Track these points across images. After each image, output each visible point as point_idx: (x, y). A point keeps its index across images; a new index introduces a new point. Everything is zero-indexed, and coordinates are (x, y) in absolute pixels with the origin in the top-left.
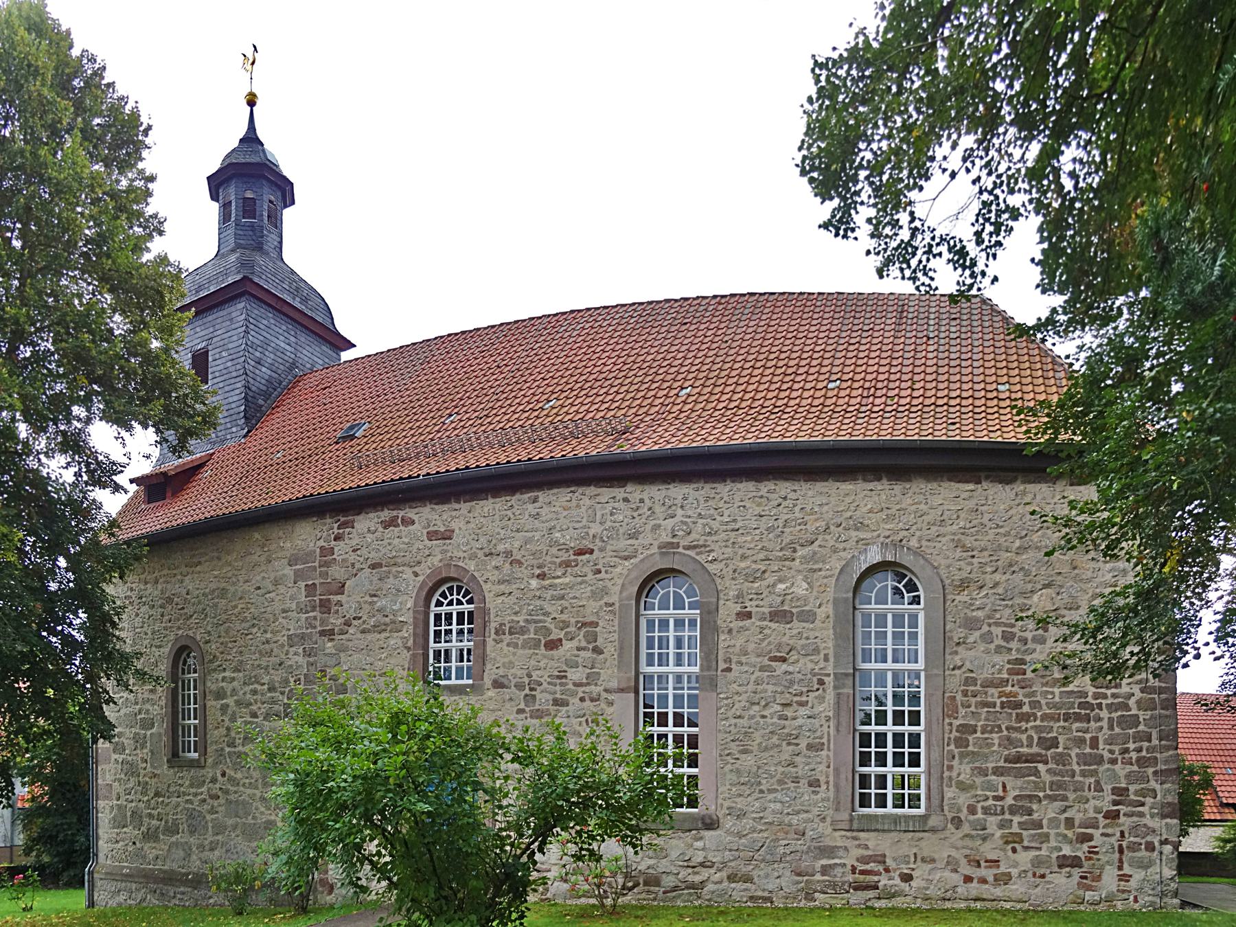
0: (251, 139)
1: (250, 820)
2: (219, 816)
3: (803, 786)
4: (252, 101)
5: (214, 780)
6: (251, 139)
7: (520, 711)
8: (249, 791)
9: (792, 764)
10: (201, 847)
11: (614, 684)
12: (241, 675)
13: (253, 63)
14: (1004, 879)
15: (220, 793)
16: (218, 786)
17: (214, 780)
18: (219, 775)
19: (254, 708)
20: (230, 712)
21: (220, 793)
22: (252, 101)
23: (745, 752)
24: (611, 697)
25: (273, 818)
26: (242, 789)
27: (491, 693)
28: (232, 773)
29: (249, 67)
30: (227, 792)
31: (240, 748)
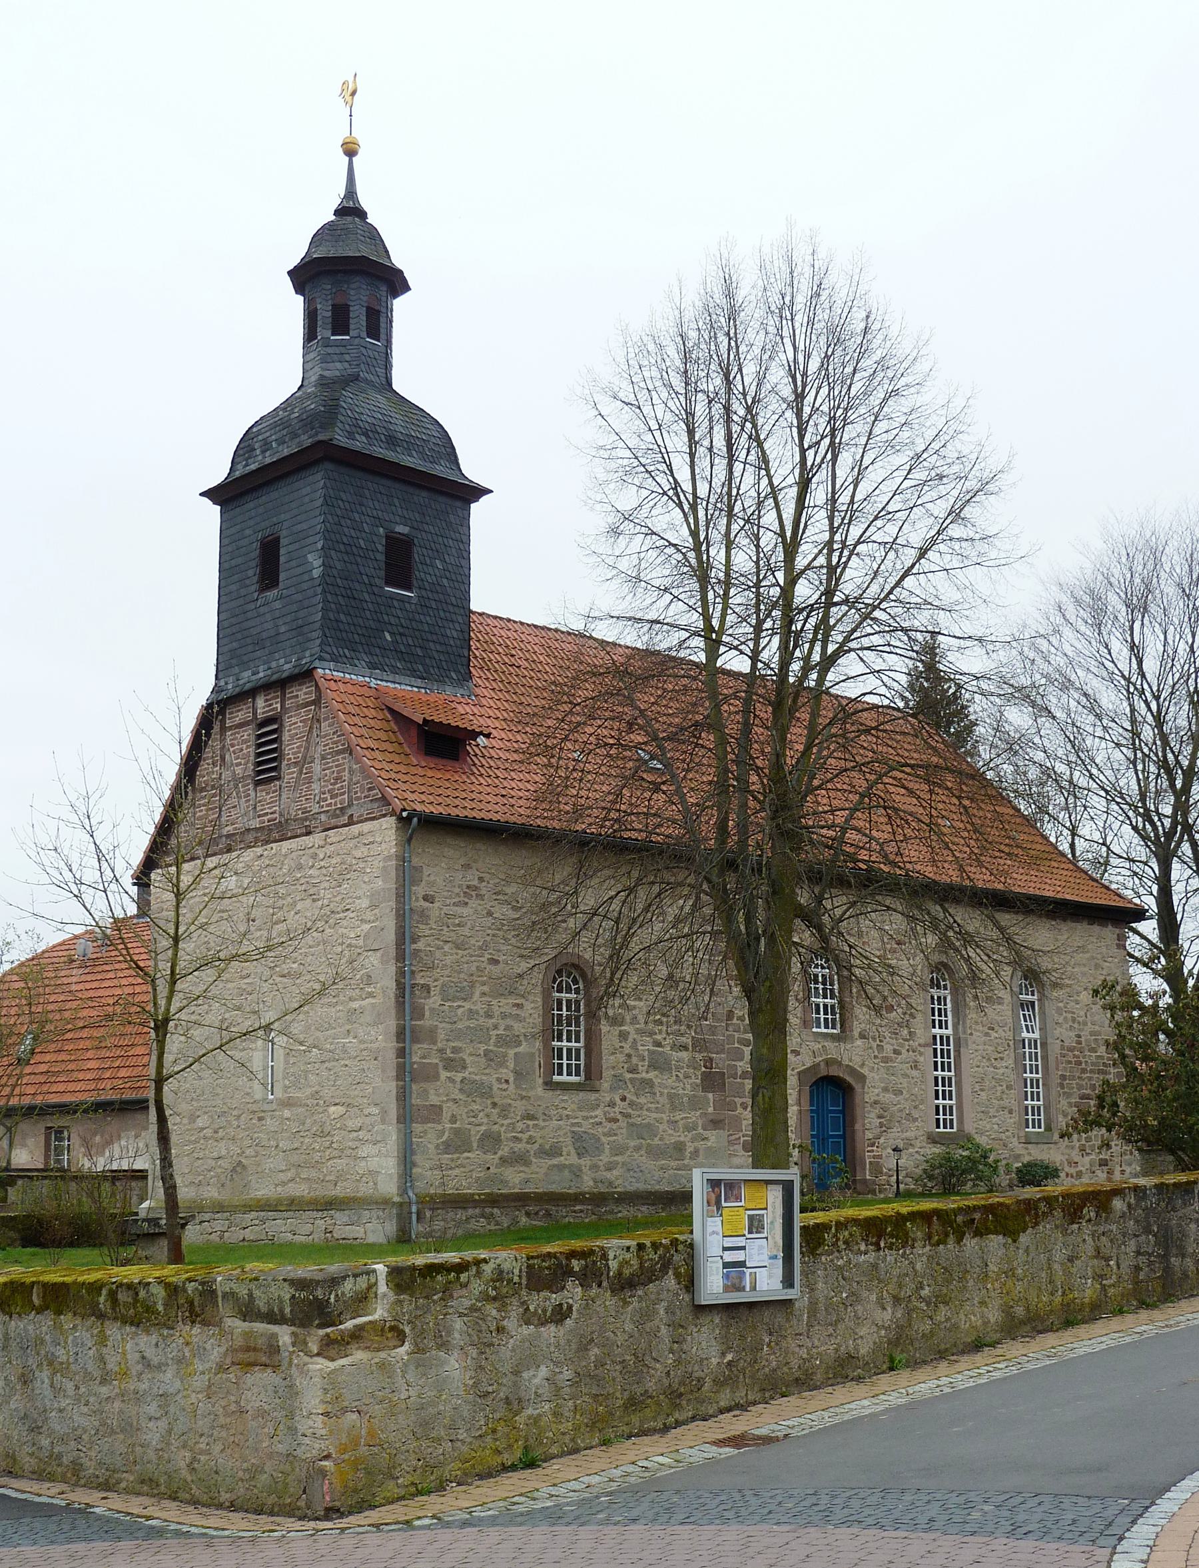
0: (350, 211)
1: (656, 1141)
2: (619, 1138)
3: (1006, 1112)
4: (350, 151)
5: (612, 1104)
6: (350, 211)
7: (876, 1057)
8: (654, 1115)
9: (1002, 1099)
10: (594, 1167)
11: (922, 1041)
12: (642, 1004)
13: (353, 93)
14: (1079, 1175)
15: (619, 1117)
16: (617, 1109)
17: (612, 1104)
18: (617, 1100)
19: (658, 1037)
20: (630, 1039)
21: (619, 1117)
22: (350, 151)
23: (982, 1090)
24: (922, 1050)
25: (682, 1139)
26: (645, 1113)
27: (859, 1042)
28: (634, 1098)
29: (349, 98)
30: (628, 1116)
31: (644, 1075)
